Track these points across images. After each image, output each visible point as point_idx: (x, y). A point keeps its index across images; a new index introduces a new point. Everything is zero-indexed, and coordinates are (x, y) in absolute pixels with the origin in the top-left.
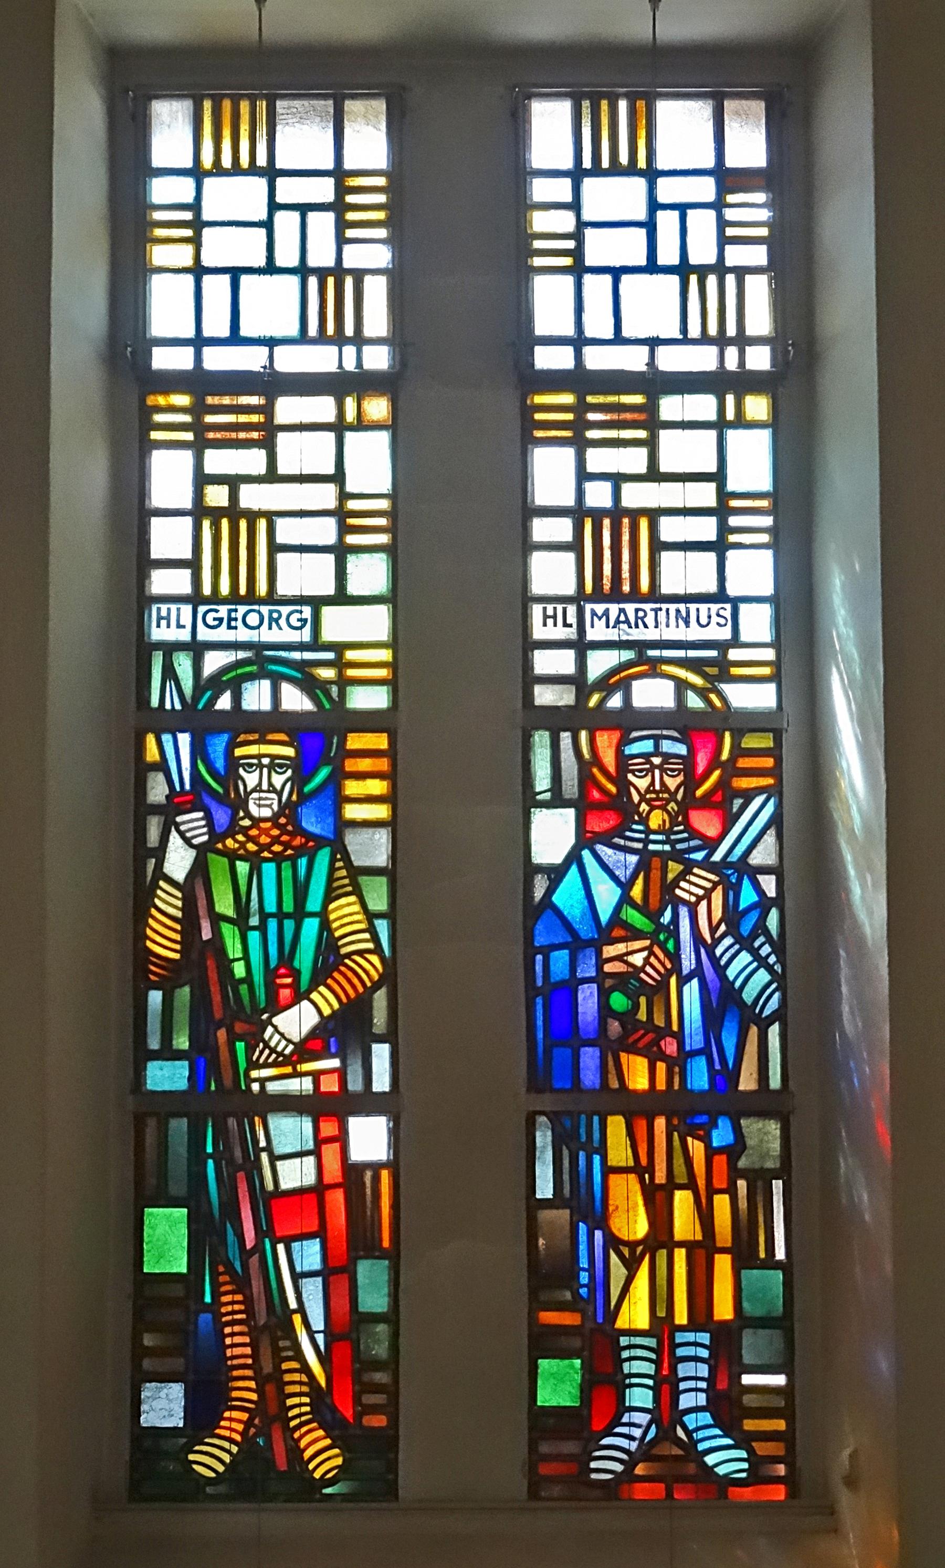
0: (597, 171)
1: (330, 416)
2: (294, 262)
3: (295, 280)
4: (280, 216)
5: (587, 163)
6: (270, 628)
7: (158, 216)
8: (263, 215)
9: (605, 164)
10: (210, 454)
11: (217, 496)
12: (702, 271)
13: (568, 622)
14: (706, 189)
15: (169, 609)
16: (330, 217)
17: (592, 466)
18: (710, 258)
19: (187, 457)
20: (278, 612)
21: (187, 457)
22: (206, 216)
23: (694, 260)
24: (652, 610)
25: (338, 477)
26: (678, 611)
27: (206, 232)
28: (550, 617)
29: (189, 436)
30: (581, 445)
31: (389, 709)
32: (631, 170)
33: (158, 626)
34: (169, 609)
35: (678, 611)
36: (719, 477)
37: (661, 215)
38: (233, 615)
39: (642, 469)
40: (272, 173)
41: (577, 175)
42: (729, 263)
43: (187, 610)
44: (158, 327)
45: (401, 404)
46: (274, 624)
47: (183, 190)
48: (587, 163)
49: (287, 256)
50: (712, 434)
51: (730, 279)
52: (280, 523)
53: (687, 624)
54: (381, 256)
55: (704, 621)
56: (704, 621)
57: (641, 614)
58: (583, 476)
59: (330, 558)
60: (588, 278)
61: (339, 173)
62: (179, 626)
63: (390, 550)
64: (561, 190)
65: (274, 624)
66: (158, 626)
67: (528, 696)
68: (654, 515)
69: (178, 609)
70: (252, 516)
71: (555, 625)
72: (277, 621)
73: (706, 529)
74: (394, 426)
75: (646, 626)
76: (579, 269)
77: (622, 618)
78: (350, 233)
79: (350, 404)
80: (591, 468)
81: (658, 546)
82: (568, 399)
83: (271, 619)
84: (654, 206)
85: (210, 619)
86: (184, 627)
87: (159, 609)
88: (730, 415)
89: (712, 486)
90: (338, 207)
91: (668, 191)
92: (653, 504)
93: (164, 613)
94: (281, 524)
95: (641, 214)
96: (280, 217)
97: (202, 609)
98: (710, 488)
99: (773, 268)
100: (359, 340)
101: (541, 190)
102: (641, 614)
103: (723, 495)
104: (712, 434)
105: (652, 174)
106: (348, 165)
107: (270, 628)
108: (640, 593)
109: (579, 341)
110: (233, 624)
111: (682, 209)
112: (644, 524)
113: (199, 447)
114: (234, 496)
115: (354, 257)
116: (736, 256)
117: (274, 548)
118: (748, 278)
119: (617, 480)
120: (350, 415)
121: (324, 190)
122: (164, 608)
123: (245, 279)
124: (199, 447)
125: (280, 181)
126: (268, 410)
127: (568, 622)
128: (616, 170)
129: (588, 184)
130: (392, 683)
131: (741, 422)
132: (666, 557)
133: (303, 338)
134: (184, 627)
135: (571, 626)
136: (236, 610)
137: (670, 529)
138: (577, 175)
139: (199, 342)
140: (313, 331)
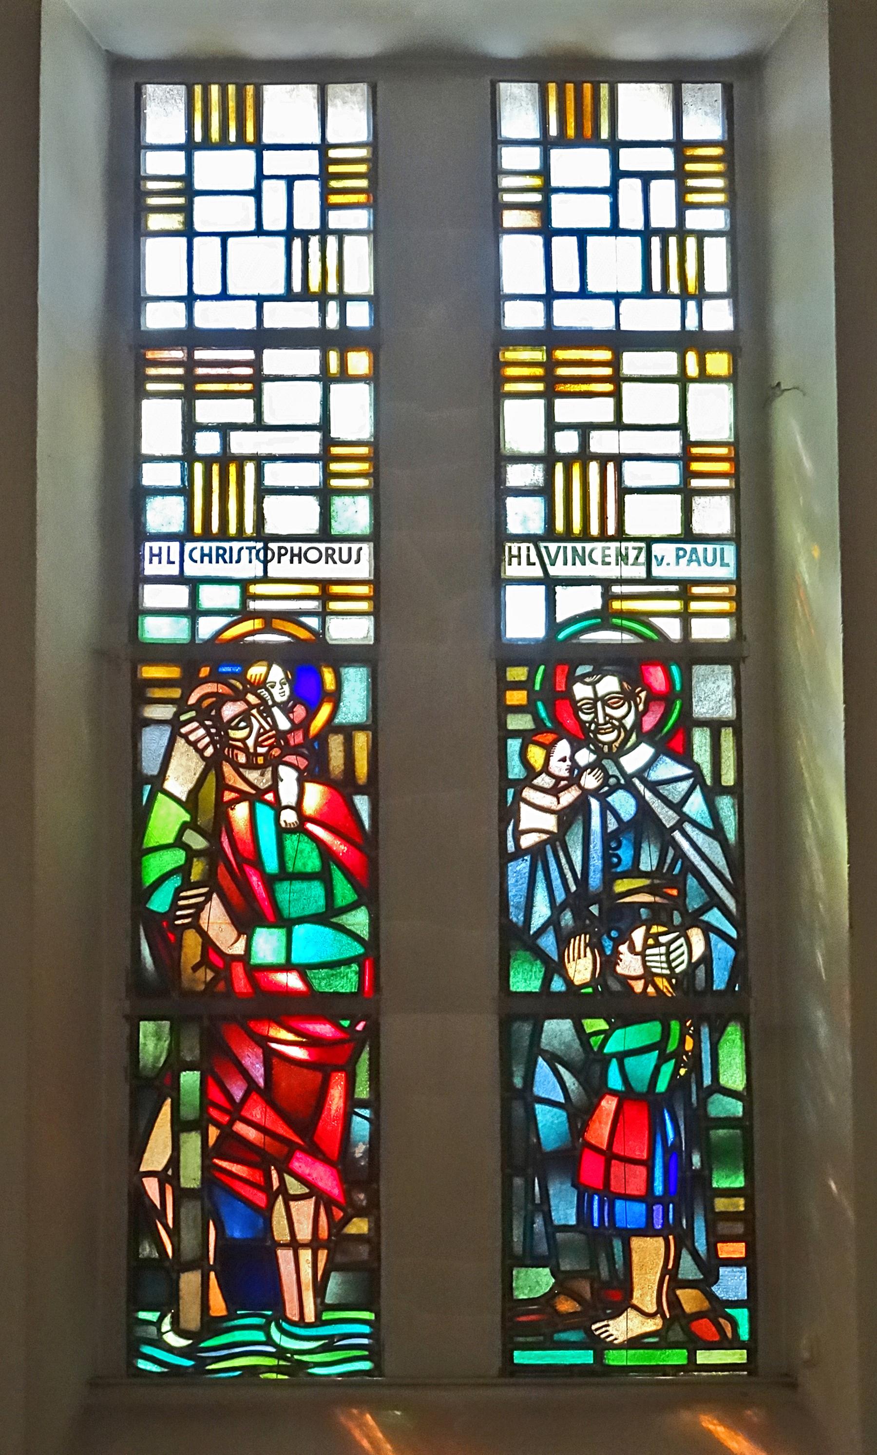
0: (207, 145)
1: (673, 370)
2: (281, 225)
3: (281, 241)
4: (623, 183)
5: (198, 137)
6: (327, 562)
7: (151, 185)
8: (606, 182)
9: (232, 138)
10: (560, 404)
11: (567, 442)
12: (664, 234)
13: (532, 561)
14: (664, 159)
15: (519, 548)
16: (315, 185)
17: (560, 417)
18: (670, 222)
19: (539, 404)
20: (285, 548)
21: (539, 404)
22: (198, 185)
23: (655, 224)
24: (634, 548)
25: (682, 426)
26: (574, 549)
27: (198, 200)
28: (515, 557)
29: (539, 387)
30: (189, 397)
31: (731, 642)
32: (241, 144)
33: (151, 562)
34: (519, 548)
35: (574, 549)
36: (324, 426)
37: (623, 183)
38: (607, 552)
39: (610, 418)
40: (259, 147)
41: (189, 148)
42: (689, 225)
43: (175, 546)
44: (152, 285)
45: (382, 358)
46: (330, 560)
47: (175, 163)
48: (198, 137)
49: (275, 220)
50: (675, 388)
51: (691, 243)
52: (627, 466)
53: (584, 564)
54: (717, 220)
55: (710, 560)
56: (710, 560)
57: (330, 552)
58: (552, 427)
59: (677, 499)
60: (556, 241)
61: (323, 147)
62: (529, 563)
63: (735, 494)
64: (531, 158)
65: (330, 560)
66: (151, 562)
67: (134, 628)
68: (260, 460)
69: (722, 550)
70: (241, 460)
71: (519, 564)
72: (223, 556)
73: (671, 474)
74: (373, 378)
75: (225, 562)
76: (189, 232)
77: (694, 557)
78: (691, 198)
79: (691, 358)
80: (559, 418)
81: (623, 491)
82: (178, 354)
83: (327, 556)
84: (617, 174)
85: (197, 555)
86: (173, 563)
87: (151, 548)
88: (334, 368)
89: (676, 434)
90: (679, 175)
91: (629, 159)
92: (263, 450)
93: (515, 552)
94: (269, 468)
95: (605, 181)
96: (624, 184)
97: (189, 546)
98: (316, 437)
99: (731, 234)
100: (702, 296)
101: (510, 158)
102: (681, 553)
103: (328, 442)
104: (675, 388)
105: (615, 145)
106: (687, 136)
107: (327, 562)
108: (573, 534)
109: (550, 297)
110: (607, 560)
111: (647, 177)
112: (611, 467)
113: (550, 395)
114: (584, 442)
115: (695, 220)
116: (336, 219)
117: (623, 491)
118: (707, 240)
119: (225, 429)
120: (693, 370)
121: (664, 159)
122: (156, 545)
123: (591, 240)
124: (550, 395)
125: (623, 152)
126: (616, 364)
127: (172, 559)
128: (224, 145)
129: (199, 156)
130: (737, 616)
131: (344, 377)
132: (270, 502)
133: (289, 296)
134: (173, 563)
135: (728, 565)
136: (609, 548)
137: (634, 473)
138: (189, 148)
139: (550, 297)
140: (657, 286)
